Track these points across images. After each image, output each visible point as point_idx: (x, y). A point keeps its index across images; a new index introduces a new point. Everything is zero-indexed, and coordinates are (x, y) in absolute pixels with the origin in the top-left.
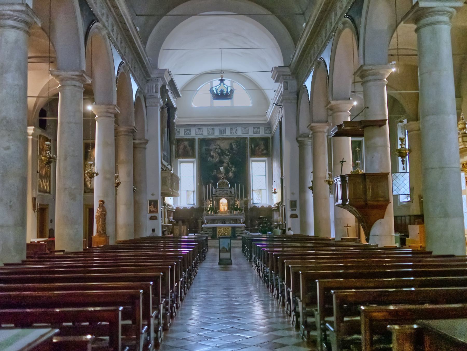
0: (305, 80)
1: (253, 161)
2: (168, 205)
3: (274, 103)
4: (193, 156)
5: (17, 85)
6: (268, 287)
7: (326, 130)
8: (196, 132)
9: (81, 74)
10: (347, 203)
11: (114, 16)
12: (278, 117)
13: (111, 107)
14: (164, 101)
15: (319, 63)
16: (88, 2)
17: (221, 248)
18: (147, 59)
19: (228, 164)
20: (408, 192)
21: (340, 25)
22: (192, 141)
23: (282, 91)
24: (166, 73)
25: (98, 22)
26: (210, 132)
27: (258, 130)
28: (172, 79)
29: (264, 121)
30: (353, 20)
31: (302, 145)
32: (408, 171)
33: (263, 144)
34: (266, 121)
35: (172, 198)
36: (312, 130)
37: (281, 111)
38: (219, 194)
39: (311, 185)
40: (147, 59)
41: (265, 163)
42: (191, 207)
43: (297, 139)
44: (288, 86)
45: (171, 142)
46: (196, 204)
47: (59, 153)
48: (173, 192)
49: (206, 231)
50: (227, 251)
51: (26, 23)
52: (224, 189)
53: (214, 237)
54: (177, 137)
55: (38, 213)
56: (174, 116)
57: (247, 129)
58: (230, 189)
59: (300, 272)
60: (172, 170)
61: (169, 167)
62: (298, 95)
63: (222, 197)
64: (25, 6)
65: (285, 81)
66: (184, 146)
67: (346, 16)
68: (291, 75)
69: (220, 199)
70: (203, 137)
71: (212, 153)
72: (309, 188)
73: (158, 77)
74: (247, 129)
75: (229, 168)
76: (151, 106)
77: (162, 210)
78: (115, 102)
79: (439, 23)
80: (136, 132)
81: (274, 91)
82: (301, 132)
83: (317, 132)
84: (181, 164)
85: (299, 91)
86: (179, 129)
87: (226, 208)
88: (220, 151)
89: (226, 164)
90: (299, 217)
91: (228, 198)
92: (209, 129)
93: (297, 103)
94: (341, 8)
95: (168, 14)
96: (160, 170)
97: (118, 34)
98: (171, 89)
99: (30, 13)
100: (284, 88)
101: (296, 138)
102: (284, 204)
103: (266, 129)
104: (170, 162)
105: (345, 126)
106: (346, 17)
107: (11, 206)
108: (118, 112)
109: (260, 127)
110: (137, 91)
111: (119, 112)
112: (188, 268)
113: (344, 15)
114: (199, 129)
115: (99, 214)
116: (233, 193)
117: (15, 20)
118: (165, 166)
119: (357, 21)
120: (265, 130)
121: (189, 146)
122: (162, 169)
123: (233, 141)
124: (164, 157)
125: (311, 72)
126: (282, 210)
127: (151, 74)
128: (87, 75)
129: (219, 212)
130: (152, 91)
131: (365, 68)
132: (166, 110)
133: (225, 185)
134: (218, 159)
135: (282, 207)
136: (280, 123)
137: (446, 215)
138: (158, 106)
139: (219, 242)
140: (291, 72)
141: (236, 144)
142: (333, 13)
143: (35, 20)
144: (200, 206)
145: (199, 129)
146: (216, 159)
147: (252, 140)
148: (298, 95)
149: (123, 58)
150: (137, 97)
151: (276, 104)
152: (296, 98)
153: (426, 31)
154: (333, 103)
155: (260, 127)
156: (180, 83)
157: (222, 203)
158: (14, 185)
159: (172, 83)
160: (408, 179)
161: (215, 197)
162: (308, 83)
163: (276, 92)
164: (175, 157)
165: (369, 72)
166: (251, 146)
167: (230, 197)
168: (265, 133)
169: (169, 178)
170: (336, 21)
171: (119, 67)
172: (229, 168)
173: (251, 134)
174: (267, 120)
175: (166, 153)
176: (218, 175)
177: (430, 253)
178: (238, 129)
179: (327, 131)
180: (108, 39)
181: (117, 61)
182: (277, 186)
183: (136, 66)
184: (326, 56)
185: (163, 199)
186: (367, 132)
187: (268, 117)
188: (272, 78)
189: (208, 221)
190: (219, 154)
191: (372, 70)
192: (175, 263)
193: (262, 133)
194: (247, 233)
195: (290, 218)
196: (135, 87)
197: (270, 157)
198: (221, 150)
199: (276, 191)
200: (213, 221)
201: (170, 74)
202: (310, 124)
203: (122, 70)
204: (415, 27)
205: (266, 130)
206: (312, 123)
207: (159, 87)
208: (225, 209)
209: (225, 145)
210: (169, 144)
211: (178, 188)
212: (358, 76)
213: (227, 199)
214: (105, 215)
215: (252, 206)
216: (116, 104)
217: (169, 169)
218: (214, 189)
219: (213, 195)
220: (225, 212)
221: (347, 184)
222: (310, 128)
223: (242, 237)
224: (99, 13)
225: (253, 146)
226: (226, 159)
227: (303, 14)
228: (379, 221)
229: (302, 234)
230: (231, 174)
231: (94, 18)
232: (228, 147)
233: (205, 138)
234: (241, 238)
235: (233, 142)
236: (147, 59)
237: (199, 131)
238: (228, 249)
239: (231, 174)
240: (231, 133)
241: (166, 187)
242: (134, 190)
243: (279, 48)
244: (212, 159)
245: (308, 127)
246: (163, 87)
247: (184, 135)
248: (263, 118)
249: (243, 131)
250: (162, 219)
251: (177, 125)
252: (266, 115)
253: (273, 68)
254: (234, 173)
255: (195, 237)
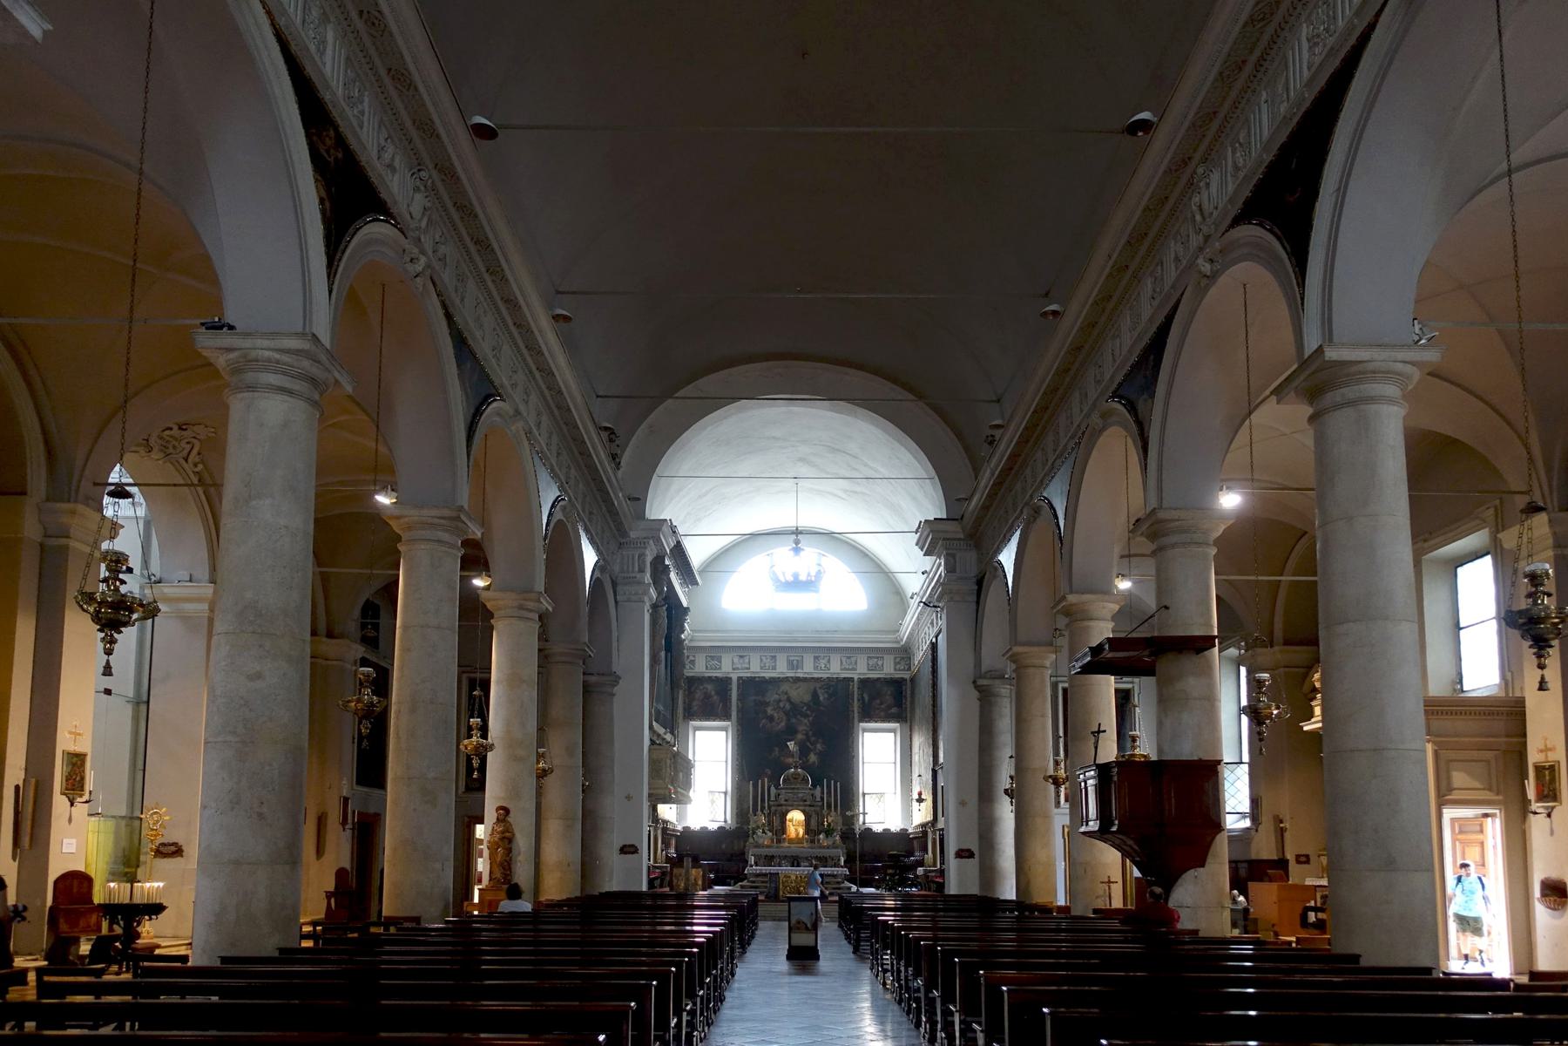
0: (999, 550)
1: (865, 730)
2: (666, 822)
3: (921, 602)
4: (727, 717)
5: (286, 527)
6: (918, 1025)
7: (1047, 663)
8: (733, 662)
9: (454, 514)
10: (1114, 829)
11: (542, 393)
12: (928, 634)
13: (533, 596)
14: (659, 592)
15: (1037, 511)
16: (477, 351)
17: (793, 921)
18: (619, 499)
19: (807, 734)
20: (1245, 807)
21: (1095, 419)
22: (723, 684)
23: (941, 574)
24: (665, 529)
25: (504, 400)
26: (767, 665)
27: (880, 663)
28: (678, 542)
29: (893, 642)
30: (1132, 407)
31: (986, 698)
32: (1246, 758)
33: (889, 693)
34: (898, 642)
35: (674, 806)
36: (1014, 662)
37: (935, 620)
38: (786, 800)
39: (1008, 786)
40: (620, 495)
41: (895, 736)
42: (718, 828)
43: (974, 682)
44: (955, 562)
45: (674, 685)
46: (729, 821)
47: (398, 695)
48: (676, 793)
49: (754, 882)
50: (807, 928)
51: (313, 381)
52: (798, 789)
53: (773, 897)
54: (688, 673)
55: (353, 833)
56: (683, 626)
57: (852, 659)
58: (810, 789)
59: (1004, 988)
60: (674, 746)
61: (668, 737)
62: (980, 583)
63: (790, 808)
64: (309, 340)
65: (950, 551)
66: (706, 693)
67: (1113, 397)
68: (963, 540)
69: (788, 812)
70: (749, 675)
71: (770, 711)
72: (1006, 791)
73: (645, 538)
74: (853, 659)
75: (808, 744)
76: (629, 600)
77: (649, 831)
78: (540, 586)
79: (1371, 400)
80: (590, 656)
81: (923, 573)
82: (984, 669)
83: (1027, 667)
84: (697, 732)
85: (983, 577)
86: (694, 656)
87: (801, 831)
88: (788, 706)
89: (803, 734)
90: (977, 856)
91: (807, 809)
92: (764, 658)
93: (978, 603)
94: (1098, 382)
95: (676, 395)
96: (647, 742)
97: (551, 433)
98: (677, 567)
99: (323, 358)
100: (946, 568)
101: (972, 680)
102: (940, 825)
103: (898, 660)
104: (672, 727)
105: (1111, 649)
106: (1113, 401)
107: (260, 815)
108: (547, 609)
109: (885, 656)
110: (595, 565)
111: (551, 609)
112: (709, 975)
113: (1107, 397)
114: (741, 657)
115: (496, 839)
116: (818, 799)
117: (284, 373)
118: (659, 735)
119: (1141, 406)
120: (896, 664)
121: (717, 693)
122: (652, 742)
123: (818, 685)
124: (656, 716)
125: (1016, 530)
126: (934, 840)
127: (631, 530)
128: (470, 519)
129: (784, 839)
130: (631, 569)
131: (1161, 515)
132: (663, 611)
133: (799, 780)
134: (783, 724)
135: (934, 833)
136: (934, 647)
137: (1390, 864)
138: (643, 602)
139: (789, 907)
140: (964, 531)
141: (827, 692)
142: (1077, 394)
143: (337, 375)
144: (739, 825)
145: (741, 657)
146: (778, 724)
147: (865, 683)
148: (980, 583)
149: (561, 489)
150: (594, 579)
151: (924, 603)
152: (975, 592)
153: (1340, 422)
154: (1072, 598)
155: (885, 656)
156: (697, 553)
157: (791, 820)
158: (270, 765)
159: (679, 552)
160: (1246, 778)
161: (774, 805)
162: (1007, 558)
163: (926, 575)
164: (685, 716)
165: (1173, 524)
166: (863, 698)
167: (812, 808)
168: (895, 669)
169: (668, 761)
170: (1084, 412)
171: (551, 508)
172: (808, 744)
173: (862, 671)
174: (902, 640)
175: (661, 708)
176: (782, 758)
177: (1356, 958)
178: (831, 659)
179: (1051, 664)
180: (526, 443)
181: (549, 494)
182: (922, 784)
183: (595, 511)
184: (1057, 496)
185: (654, 809)
186: (1165, 664)
187: (904, 634)
188: (917, 545)
189: (758, 858)
190: (787, 714)
191: (1178, 520)
192: (673, 969)
193: (888, 669)
194: (850, 888)
195: (956, 857)
196: (590, 557)
197: (906, 721)
198: (791, 703)
199: (923, 797)
200: (769, 860)
201: (674, 532)
202: (1011, 649)
203: (558, 515)
204: (1309, 411)
205: (899, 663)
206: (1016, 644)
207: (649, 559)
208: (798, 834)
209: (800, 694)
210: (668, 688)
211: (687, 784)
212: (1142, 534)
213: (804, 812)
214: (510, 840)
215: (863, 828)
216: (543, 590)
217: (668, 742)
218: (773, 788)
219: (771, 803)
220: (798, 840)
221: (1113, 785)
222: (1011, 656)
223: (841, 897)
224: (506, 382)
225: (866, 698)
226: (804, 725)
227: (998, 401)
228: (1191, 873)
229: (985, 894)
230: (813, 758)
231: (494, 391)
232: (807, 698)
233: (755, 677)
234: (837, 898)
235: (820, 688)
236: (620, 495)
237: (741, 661)
238: (809, 925)
239: (813, 758)
240: (816, 668)
241: (661, 781)
242: (583, 785)
243: (936, 477)
244: (771, 722)
245: (1003, 655)
246: (658, 560)
247: (704, 670)
248: (891, 637)
249: (844, 663)
250: (649, 853)
251: (690, 648)
252: (898, 631)
253: (921, 522)
254: (820, 754)
255: (727, 896)
